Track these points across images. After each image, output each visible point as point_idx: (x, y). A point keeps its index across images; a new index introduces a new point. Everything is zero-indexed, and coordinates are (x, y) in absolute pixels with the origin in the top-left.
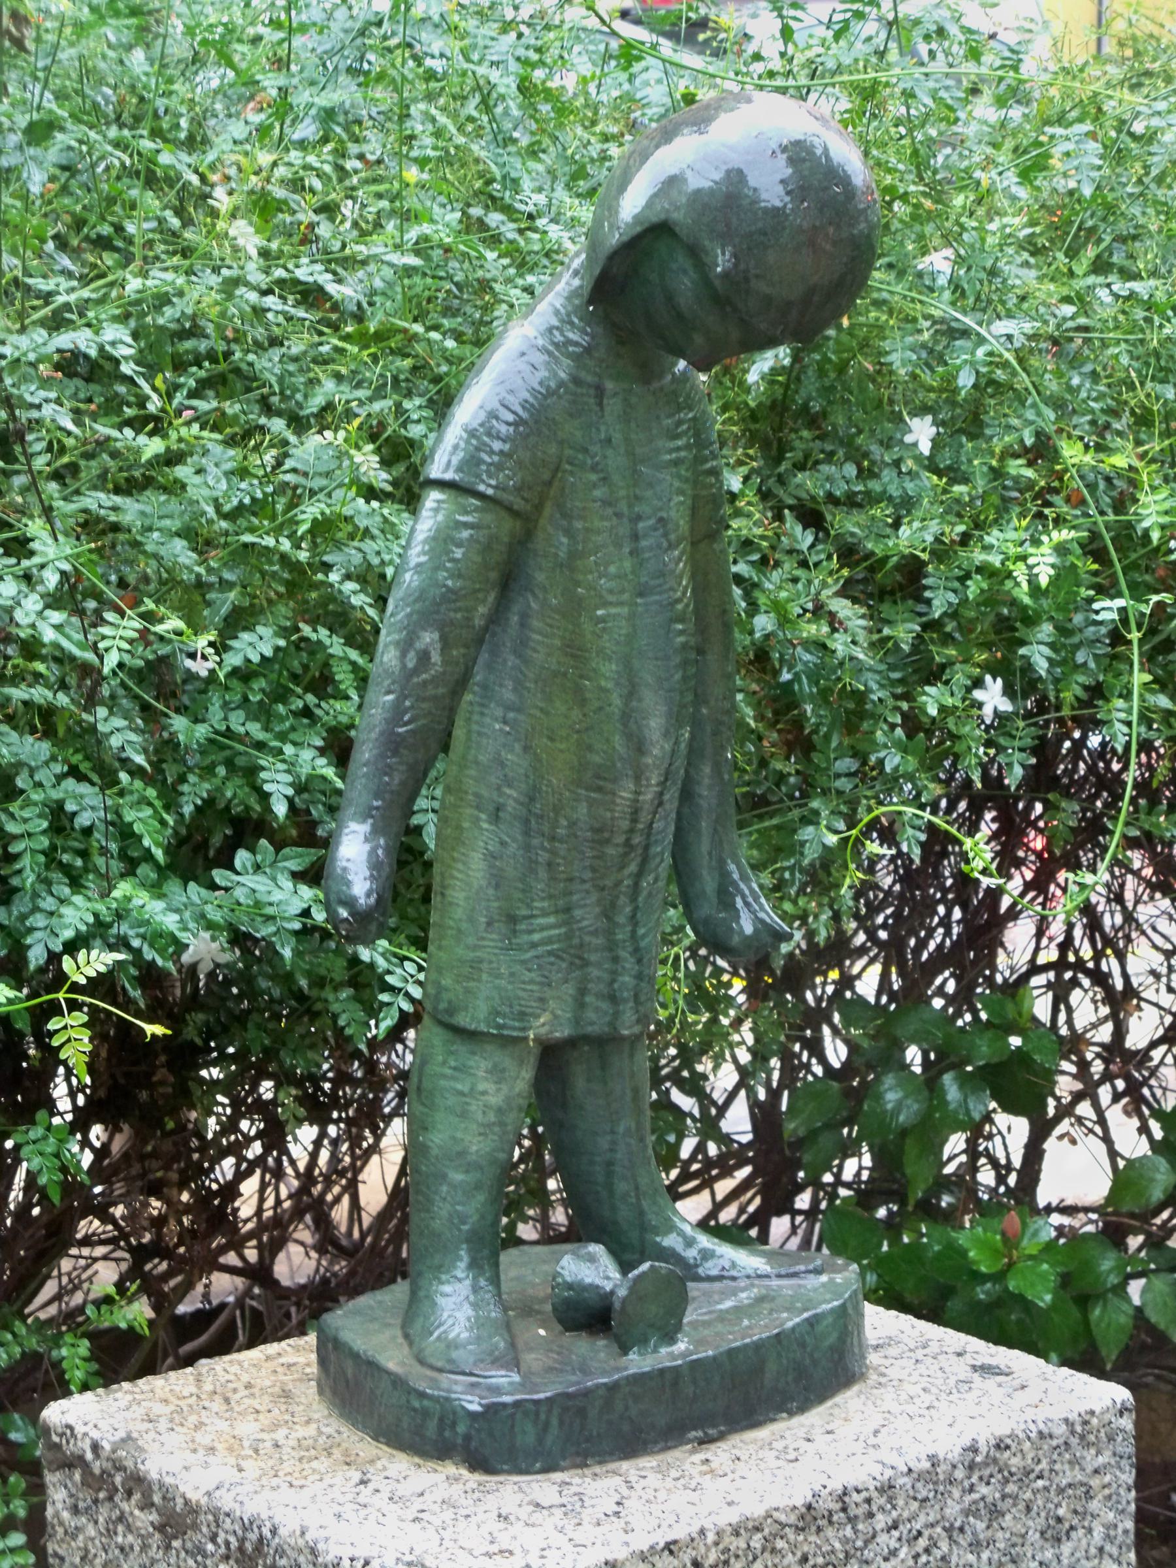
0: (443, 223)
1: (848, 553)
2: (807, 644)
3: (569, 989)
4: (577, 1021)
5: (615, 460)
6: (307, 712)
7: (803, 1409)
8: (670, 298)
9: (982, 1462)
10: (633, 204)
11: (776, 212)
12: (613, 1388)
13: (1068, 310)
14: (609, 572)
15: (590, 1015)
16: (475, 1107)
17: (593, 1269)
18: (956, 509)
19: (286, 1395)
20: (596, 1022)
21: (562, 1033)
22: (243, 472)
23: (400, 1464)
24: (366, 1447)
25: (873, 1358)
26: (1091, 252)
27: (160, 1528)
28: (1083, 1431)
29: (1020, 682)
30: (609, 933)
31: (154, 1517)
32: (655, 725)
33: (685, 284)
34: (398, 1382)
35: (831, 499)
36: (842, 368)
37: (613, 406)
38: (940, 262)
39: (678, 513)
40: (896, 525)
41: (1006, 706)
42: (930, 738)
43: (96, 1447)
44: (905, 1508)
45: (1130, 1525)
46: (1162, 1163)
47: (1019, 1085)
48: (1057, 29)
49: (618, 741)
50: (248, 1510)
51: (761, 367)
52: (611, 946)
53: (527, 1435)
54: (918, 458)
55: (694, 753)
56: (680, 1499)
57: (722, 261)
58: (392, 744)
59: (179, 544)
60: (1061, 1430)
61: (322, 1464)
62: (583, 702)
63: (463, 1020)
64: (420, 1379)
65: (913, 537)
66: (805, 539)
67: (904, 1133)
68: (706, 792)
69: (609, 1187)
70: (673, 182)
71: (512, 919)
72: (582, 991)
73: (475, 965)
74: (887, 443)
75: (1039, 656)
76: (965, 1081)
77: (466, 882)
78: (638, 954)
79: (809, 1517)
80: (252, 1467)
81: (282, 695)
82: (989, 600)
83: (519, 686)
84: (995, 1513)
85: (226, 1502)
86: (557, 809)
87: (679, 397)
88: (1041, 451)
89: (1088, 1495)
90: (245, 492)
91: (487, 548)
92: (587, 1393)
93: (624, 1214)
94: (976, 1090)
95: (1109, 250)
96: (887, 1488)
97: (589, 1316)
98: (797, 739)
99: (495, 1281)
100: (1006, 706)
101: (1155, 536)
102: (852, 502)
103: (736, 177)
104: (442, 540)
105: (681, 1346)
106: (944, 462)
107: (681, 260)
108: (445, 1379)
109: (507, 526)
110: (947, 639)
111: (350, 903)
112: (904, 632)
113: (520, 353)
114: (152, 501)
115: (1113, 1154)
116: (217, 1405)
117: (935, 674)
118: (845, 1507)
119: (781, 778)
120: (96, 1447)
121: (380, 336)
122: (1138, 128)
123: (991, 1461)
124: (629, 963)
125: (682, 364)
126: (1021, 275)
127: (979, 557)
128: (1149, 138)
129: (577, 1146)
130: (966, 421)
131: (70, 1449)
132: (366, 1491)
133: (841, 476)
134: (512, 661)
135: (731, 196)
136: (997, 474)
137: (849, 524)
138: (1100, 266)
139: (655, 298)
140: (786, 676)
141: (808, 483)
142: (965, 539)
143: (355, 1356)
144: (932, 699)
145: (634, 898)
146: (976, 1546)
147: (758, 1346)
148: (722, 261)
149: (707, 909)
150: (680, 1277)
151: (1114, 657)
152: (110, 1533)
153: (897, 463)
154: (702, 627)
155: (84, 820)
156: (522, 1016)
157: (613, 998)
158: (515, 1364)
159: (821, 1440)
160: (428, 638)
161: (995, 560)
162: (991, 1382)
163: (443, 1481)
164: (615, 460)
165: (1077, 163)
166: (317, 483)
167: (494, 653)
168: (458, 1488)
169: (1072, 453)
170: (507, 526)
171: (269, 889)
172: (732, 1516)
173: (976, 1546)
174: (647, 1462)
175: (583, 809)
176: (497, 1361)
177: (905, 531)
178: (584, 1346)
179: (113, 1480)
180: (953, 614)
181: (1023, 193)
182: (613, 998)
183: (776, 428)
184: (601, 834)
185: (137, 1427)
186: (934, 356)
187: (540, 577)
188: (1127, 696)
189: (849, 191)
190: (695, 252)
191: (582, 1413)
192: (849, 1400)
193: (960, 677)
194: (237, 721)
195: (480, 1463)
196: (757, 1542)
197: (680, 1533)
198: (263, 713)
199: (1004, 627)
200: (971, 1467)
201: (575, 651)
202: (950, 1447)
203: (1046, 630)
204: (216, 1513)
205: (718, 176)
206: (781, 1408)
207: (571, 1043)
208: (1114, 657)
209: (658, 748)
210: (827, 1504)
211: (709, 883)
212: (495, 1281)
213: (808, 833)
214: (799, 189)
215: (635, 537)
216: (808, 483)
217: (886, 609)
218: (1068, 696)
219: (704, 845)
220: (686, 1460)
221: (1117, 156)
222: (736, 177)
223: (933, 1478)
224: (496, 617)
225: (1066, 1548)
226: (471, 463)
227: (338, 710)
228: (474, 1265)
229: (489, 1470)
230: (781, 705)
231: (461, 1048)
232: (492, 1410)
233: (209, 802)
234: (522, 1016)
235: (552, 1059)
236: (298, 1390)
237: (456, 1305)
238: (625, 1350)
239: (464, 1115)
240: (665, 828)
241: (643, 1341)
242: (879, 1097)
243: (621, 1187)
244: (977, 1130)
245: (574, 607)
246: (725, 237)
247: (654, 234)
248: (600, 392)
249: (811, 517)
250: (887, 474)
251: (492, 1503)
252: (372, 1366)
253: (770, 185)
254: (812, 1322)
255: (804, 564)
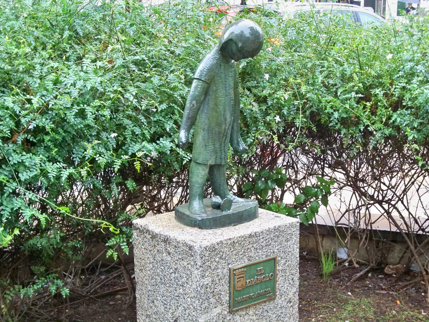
0: (192, 41)
1: (255, 96)
2: (248, 109)
3: (214, 157)
4: (215, 162)
5: (223, 76)
6: (171, 118)
7: (249, 221)
8: (232, 50)
9: (276, 229)
10: (226, 36)
11: (248, 37)
12: (221, 217)
13: (290, 57)
14: (221, 93)
15: (217, 161)
16: (200, 175)
17: (217, 199)
18: (272, 89)
19: (170, 219)
20: (218, 162)
21: (213, 164)
22: (161, 80)
23: (188, 228)
24: (183, 226)
25: (260, 215)
26: (294, 48)
27: (151, 238)
28: (292, 225)
29: (282, 116)
30: (221, 148)
31: (150, 236)
32: (228, 116)
33: (234, 48)
34: (188, 216)
35: (253, 87)
36: (254, 66)
37: (222, 67)
38: (270, 49)
39: (232, 84)
40: (263, 91)
41: (280, 120)
42: (268, 125)
43: (141, 226)
44: (265, 235)
45: (298, 240)
46: (303, 195)
47: (281, 183)
48: (288, 13)
49: (222, 118)
50: (166, 234)
51: (243, 63)
52: (221, 150)
53: (208, 223)
54: (266, 80)
55: (234, 121)
56: (231, 233)
57: (240, 45)
58: (188, 118)
59: (152, 90)
60: (288, 225)
61: (176, 228)
62: (217, 113)
63: (198, 161)
64: (191, 215)
65: (266, 92)
66: (248, 93)
67: (262, 190)
68: (235, 128)
69: (220, 188)
70: (232, 33)
71: (206, 146)
72: (216, 157)
73: (200, 153)
74: (261, 78)
75: (285, 112)
76: (271, 182)
77: (199, 141)
78: (225, 152)
79: (250, 236)
80: (166, 229)
81: (167, 115)
82: (277, 103)
83: (207, 110)
84: (278, 237)
85: (162, 233)
86: (213, 129)
87: (232, 66)
88: (286, 80)
89: (292, 235)
90: (162, 82)
91: (203, 89)
92: (217, 217)
93: (222, 192)
94: (274, 183)
95: (296, 49)
96: (262, 232)
97: (217, 207)
98: (246, 124)
99: (202, 201)
100: (280, 120)
101: (304, 93)
102: (256, 87)
103: (242, 32)
104: (196, 87)
105: (231, 211)
106: (271, 81)
107: (234, 45)
108: (195, 216)
109: (206, 85)
110: (271, 109)
111: (182, 142)
112: (264, 108)
113: (209, 58)
114: (147, 84)
115: (295, 195)
116: (159, 220)
117: (269, 115)
118: (256, 235)
119: (244, 131)
120: (141, 226)
121: (182, 59)
122: (302, 29)
123: (278, 229)
124: (223, 153)
125: (233, 61)
126: (283, 52)
127: (276, 96)
128: (303, 31)
129: (213, 183)
130: (274, 75)
131: (137, 227)
132: (183, 232)
133: (254, 83)
134: (206, 106)
135: (241, 35)
136: (279, 83)
137: (255, 91)
138: (295, 51)
139: (229, 51)
140: (245, 114)
141: (249, 84)
142: (274, 93)
143: (181, 212)
144: (268, 118)
145: (224, 143)
146: (275, 242)
147: (243, 211)
148: (240, 45)
149: (235, 145)
150: (230, 203)
151: (297, 113)
152: (143, 239)
153: (263, 81)
154: (235, 102)
155: (137, 133)
156: (207, 161)
157: (221, 159)
158: (206, 213)
159: (252, 226)
160: (194, 102)
161: (278, 96)
162: (278, 218)
163: (195, 230)
164: (223, 76)
165: (292, 34)
166: (172, 81)
167: (204, 105)
168: (197, 232)
169: (291, 80)
170: (206, 85)
171: (166, 144)
172: (239, 235)
173: (275, 242)
174: (226, 228)
175: (217, 129)
176: (203, 213)
177: (264, 92)
178: (216, 211)
179: (144, 231)
180: (272, 105)
181: (283, 39)
182: (221, 159)
183: (245, 75)
184: (220, 133)
185: (148, 223)
186: (269, 64)
187: (211, 93)
188: (299, 119)
189: (259, 35)
190: (236, 44)
191: (216, 220)
192: (256, 220)
193: (272, 115)
194: (161, 118)
195: (200, 228)
196: (243, 239)
197: (231, 237)
198: (164, 117)
199: (279, 109)
200: (275, 230)
201: (216, 105)
202: (272, 227)
203: (286, 108)
204: (160, 235)
205: (240, 32)
206: (246, 221)
207: (214, 165)
208: (297, 113)
209: (229, 120)
210: (253, 234)
211: (236, 142)
212: (202, 201)
213: (248, 139)
214: (252, 34)
215: (226, 87)
216: (249, 84)
217: (261, 105)
218: (289, 119)
219: (235, 136)
220: (231, 228)
221: (298, 33)
222: (242, 32)
223: (269, 231)
224: (204, 99)
225: (289, 243)
226: (201, 75)
227: (177, 117)
228: (199, 199)
229: (202, 229)
230: (244, 118)
231: (197, 165)
232: (202, 220)
233: (155, 131)
234: (207, 161)
235: (212, 168)
236: (171, 219)
237: (196, 204)
238: (222, 211)
239: (198, 176)
240: (229, 132)
241: (225, 210)
242: (258, 184)
243: (221, 188)
244: (273, 190)
245: (216, 98)
246: (241, 41)
247: (230, 41)
248: (221, 65)
249: (249, 89)
250: (261, 83)
251: (202, 233)
252: (184, 214)
253: (247, 33)
254: (251, 208)
255: (248, 97)
